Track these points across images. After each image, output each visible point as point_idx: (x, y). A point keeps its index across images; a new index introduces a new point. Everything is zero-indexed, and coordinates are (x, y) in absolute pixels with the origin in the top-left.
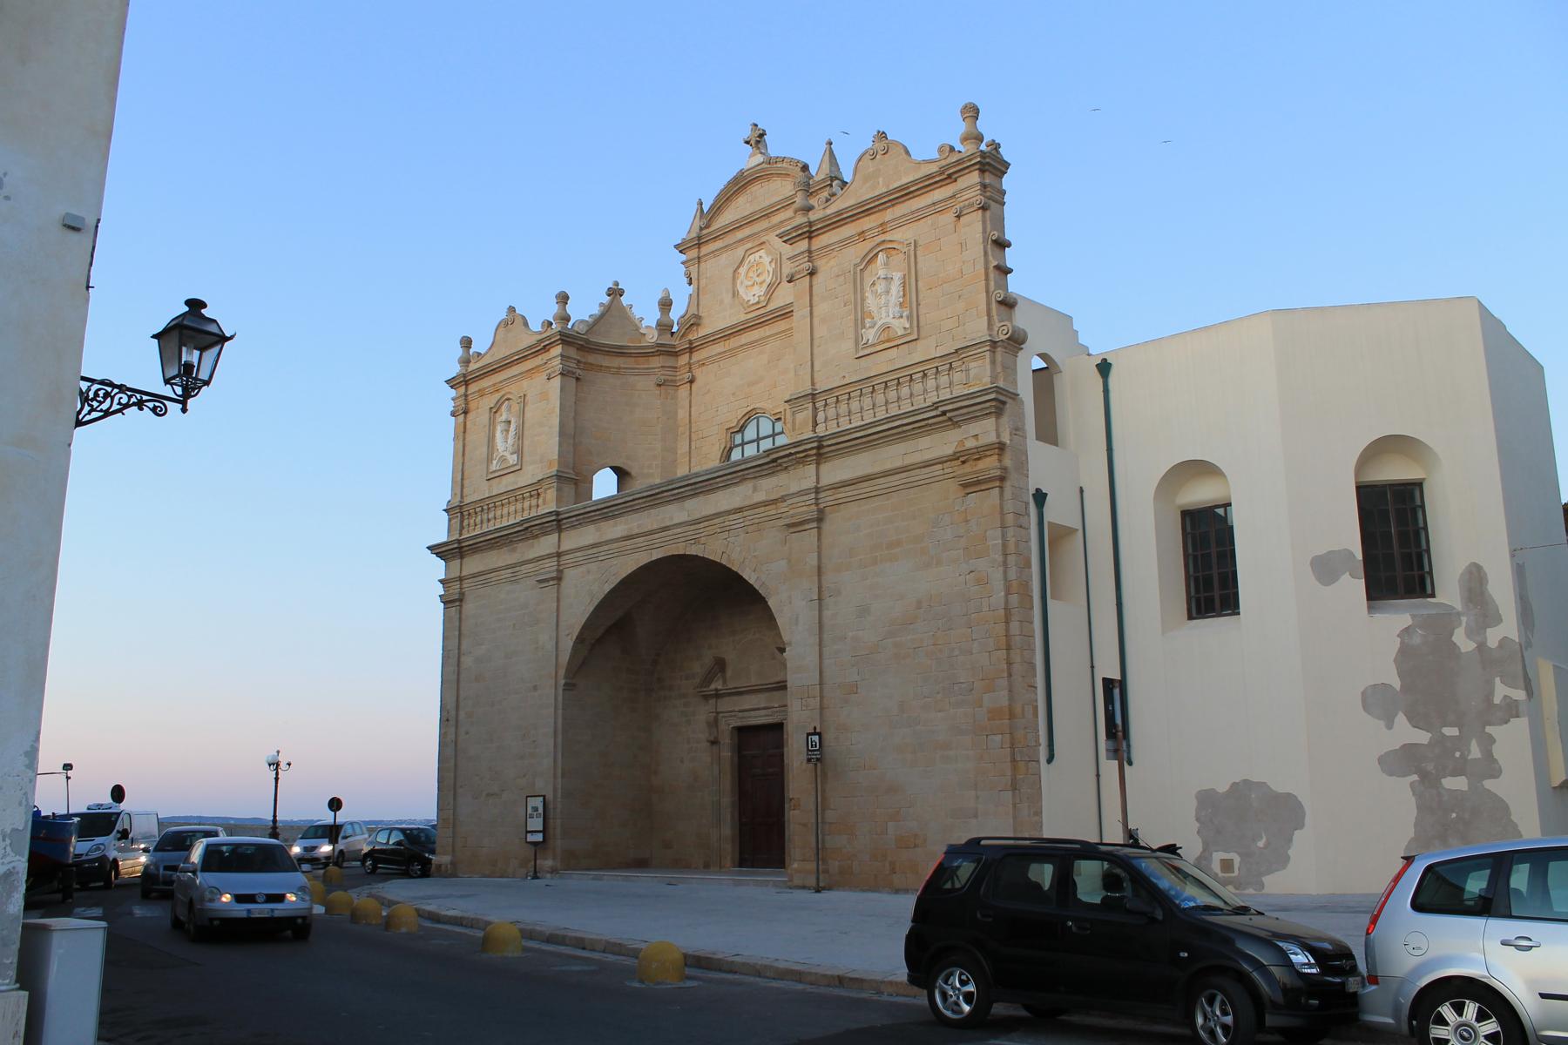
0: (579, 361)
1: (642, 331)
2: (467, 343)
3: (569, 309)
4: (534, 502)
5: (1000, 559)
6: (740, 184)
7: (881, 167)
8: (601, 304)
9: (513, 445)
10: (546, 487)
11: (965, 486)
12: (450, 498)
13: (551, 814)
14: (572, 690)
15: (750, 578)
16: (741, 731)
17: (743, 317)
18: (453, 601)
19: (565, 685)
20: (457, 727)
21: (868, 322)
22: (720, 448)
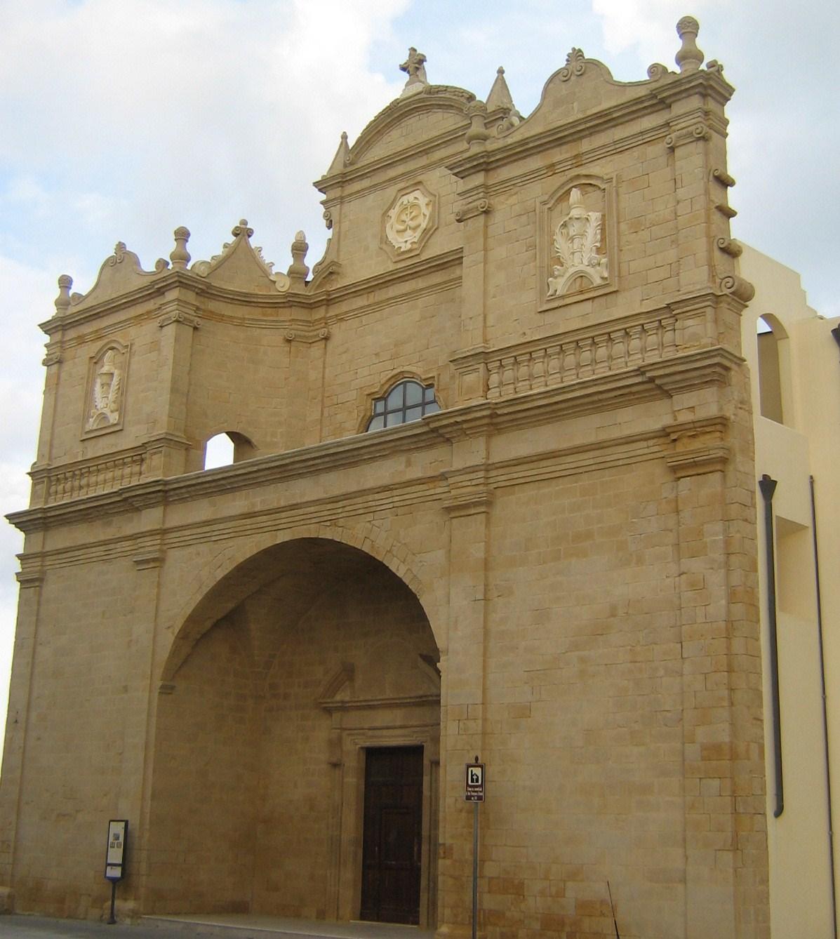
0: (198, 308)
1: (272, 278)
2: (65, 283)
3: (190, 247)
4: (136, 469)
5: (722, 558)
6: (393, 116)
8: (225, 246)
9: (114, 402)
10: (151, 452)
11: (674, 469)
12: (35, 460)
15: (398, 570)
17: (392, 267)
18: (30, 581)
19: (162, 687)
20: (26, 731)
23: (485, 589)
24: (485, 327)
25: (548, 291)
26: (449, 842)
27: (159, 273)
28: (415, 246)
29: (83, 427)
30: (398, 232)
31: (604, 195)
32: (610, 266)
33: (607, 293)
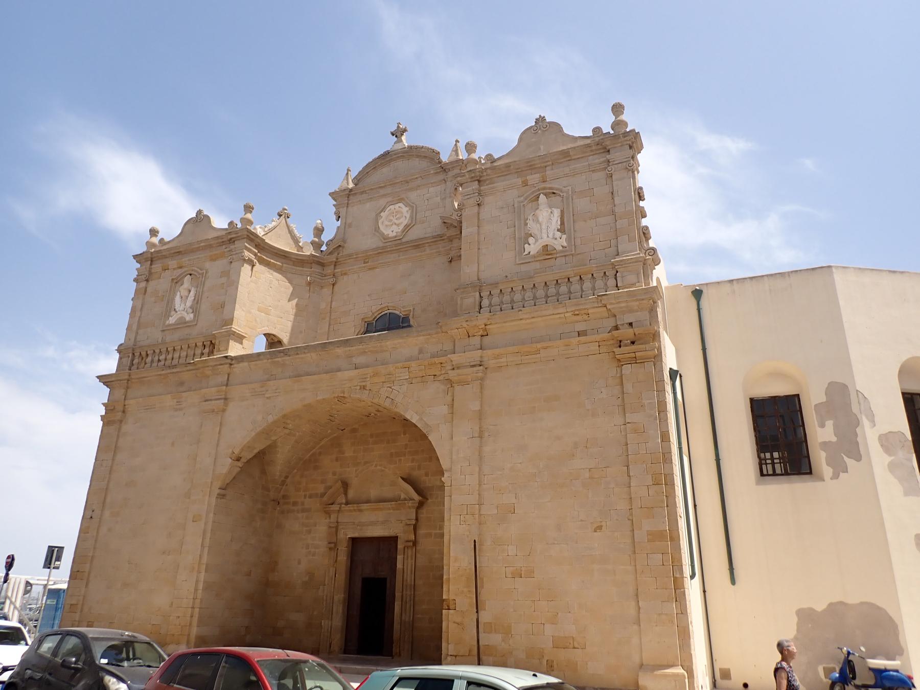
6: (386, 158)
9: (191, 308)
16: (354, 540)
21: (531, 240)
24: (478, 271)
26: (452, 597)
28: (399, 234)
30: (386, 226)
32: (568, 240)
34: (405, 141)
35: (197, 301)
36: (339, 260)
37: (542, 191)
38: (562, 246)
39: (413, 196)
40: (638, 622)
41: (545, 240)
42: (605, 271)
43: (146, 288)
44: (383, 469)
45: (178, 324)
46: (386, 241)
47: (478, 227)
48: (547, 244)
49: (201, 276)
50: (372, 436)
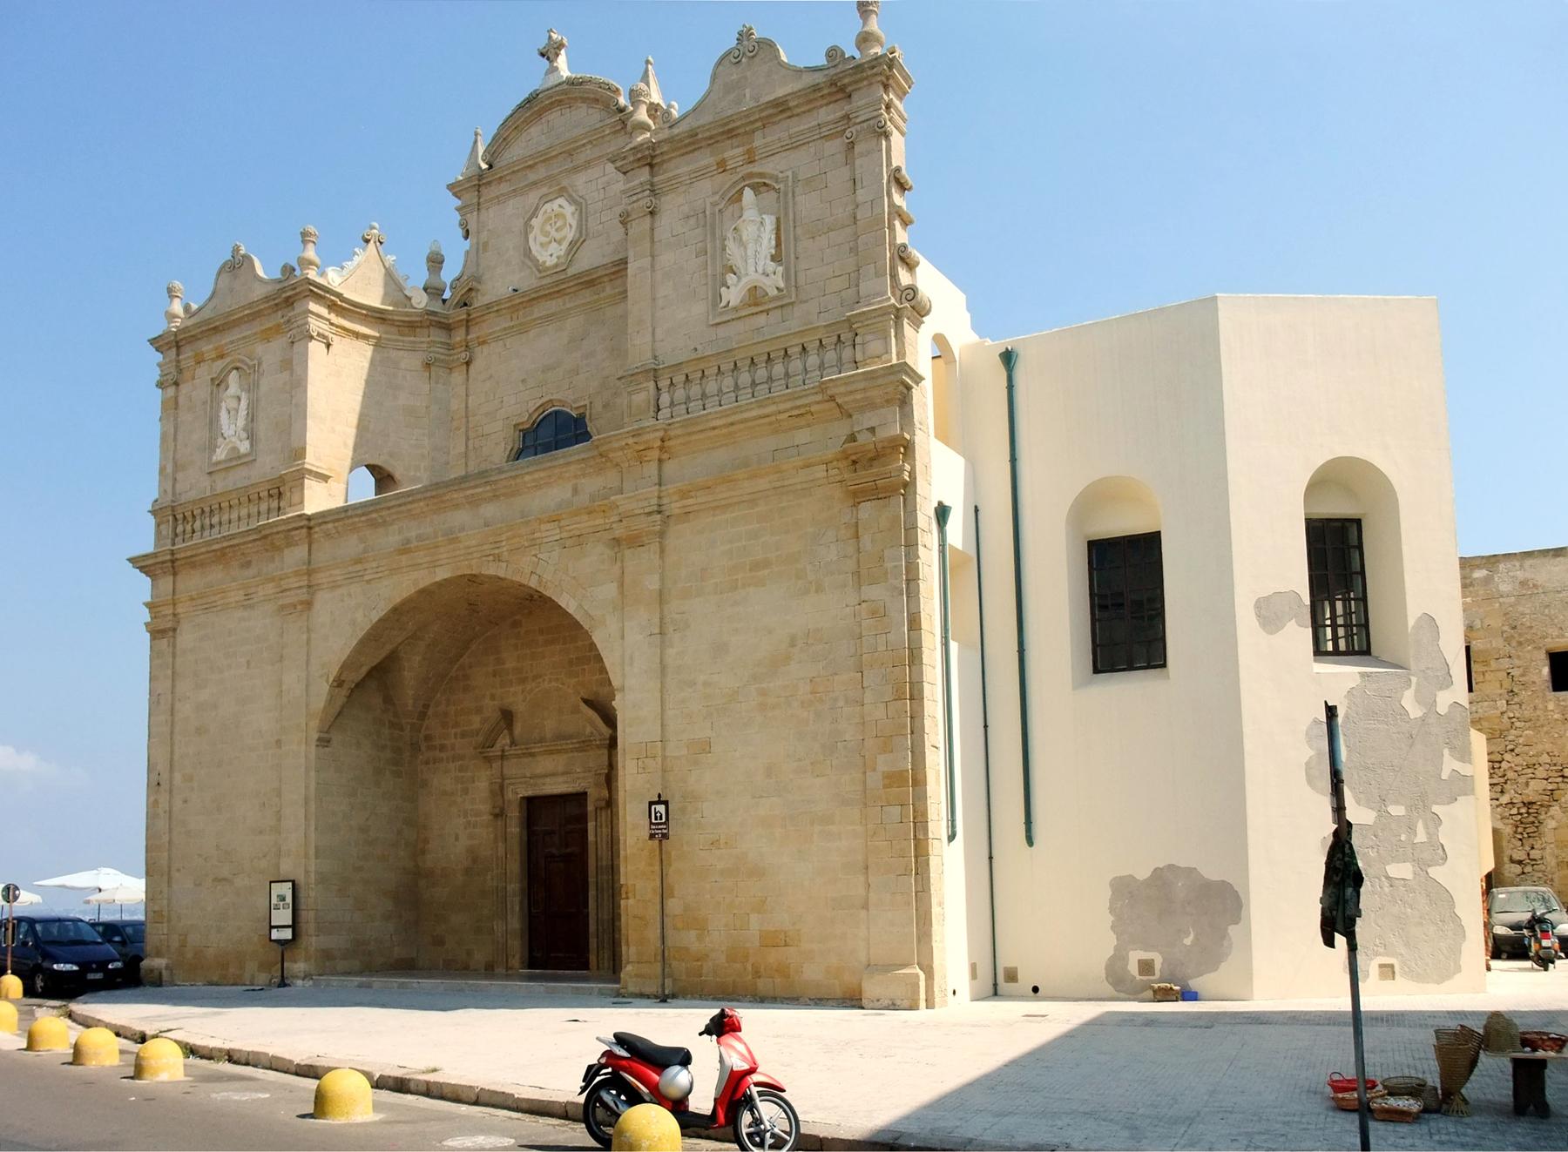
4: (274, 504)
6: (534, 107)
7: (749, 74)
9: (244, 430)
11: (855, 494)
12: (156, 496)
13: (302, 905)
14: (327, 746)
18: (162, 631)
19: (319, 739)
20: (171, 791)
21: (731, 278)
22: (505, 449)
23: (661, 622)
24: (654, 341)
25: (721, 301)
27: (286, 280)
28: (562, 260)
29: (210, 459)
30: (542, 244)
31: (779, 197)
32: (786, 277)
33: (783, 303)
34: (564, 67)
35: (252, 417)
36: (471, 317)
37: (747, 183)
38: (777, 288)
39: (580, 180)
40: (865, 906)
41: (751, 277)
42: (839, 332)
43: (176, 398)
44: (561, 686)
45: (231, 460)
46: (542, 275)
47: (653, 256)
48: (755, 284)
49: (252, 371)
50: (541, 632)
